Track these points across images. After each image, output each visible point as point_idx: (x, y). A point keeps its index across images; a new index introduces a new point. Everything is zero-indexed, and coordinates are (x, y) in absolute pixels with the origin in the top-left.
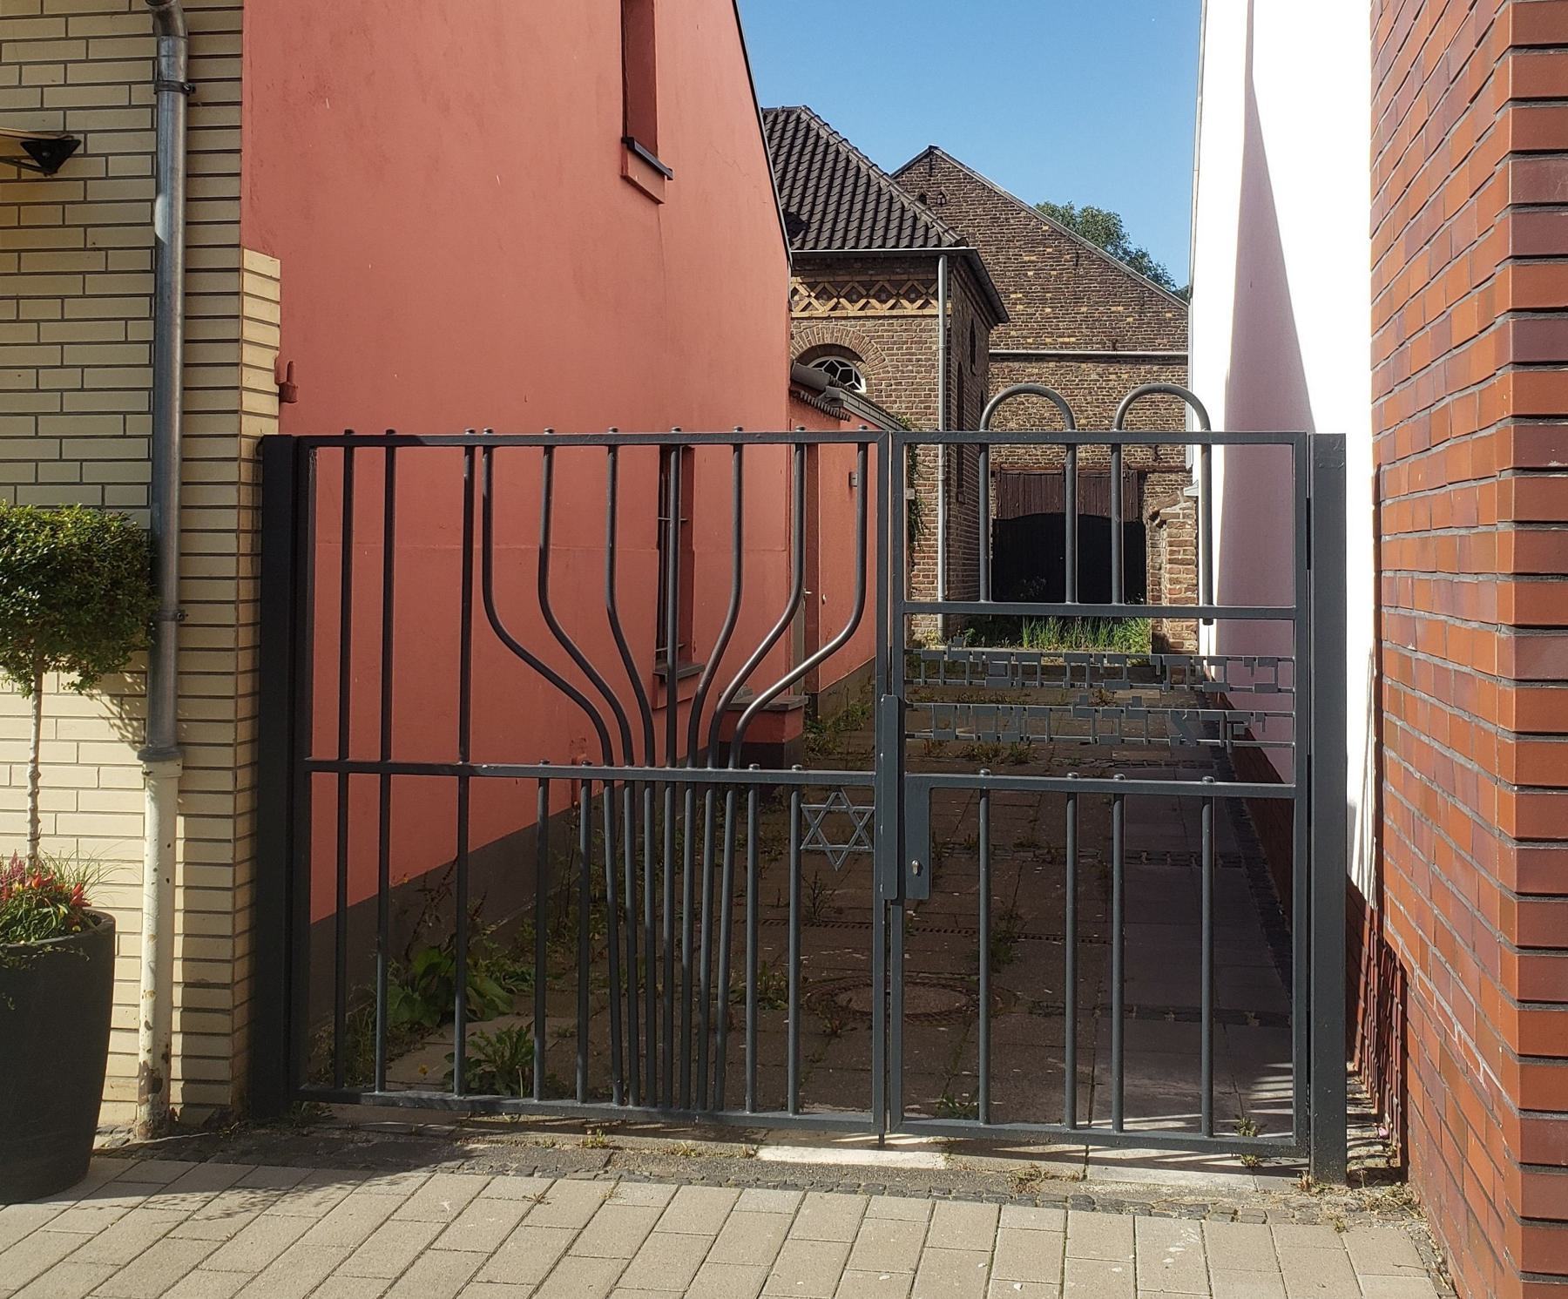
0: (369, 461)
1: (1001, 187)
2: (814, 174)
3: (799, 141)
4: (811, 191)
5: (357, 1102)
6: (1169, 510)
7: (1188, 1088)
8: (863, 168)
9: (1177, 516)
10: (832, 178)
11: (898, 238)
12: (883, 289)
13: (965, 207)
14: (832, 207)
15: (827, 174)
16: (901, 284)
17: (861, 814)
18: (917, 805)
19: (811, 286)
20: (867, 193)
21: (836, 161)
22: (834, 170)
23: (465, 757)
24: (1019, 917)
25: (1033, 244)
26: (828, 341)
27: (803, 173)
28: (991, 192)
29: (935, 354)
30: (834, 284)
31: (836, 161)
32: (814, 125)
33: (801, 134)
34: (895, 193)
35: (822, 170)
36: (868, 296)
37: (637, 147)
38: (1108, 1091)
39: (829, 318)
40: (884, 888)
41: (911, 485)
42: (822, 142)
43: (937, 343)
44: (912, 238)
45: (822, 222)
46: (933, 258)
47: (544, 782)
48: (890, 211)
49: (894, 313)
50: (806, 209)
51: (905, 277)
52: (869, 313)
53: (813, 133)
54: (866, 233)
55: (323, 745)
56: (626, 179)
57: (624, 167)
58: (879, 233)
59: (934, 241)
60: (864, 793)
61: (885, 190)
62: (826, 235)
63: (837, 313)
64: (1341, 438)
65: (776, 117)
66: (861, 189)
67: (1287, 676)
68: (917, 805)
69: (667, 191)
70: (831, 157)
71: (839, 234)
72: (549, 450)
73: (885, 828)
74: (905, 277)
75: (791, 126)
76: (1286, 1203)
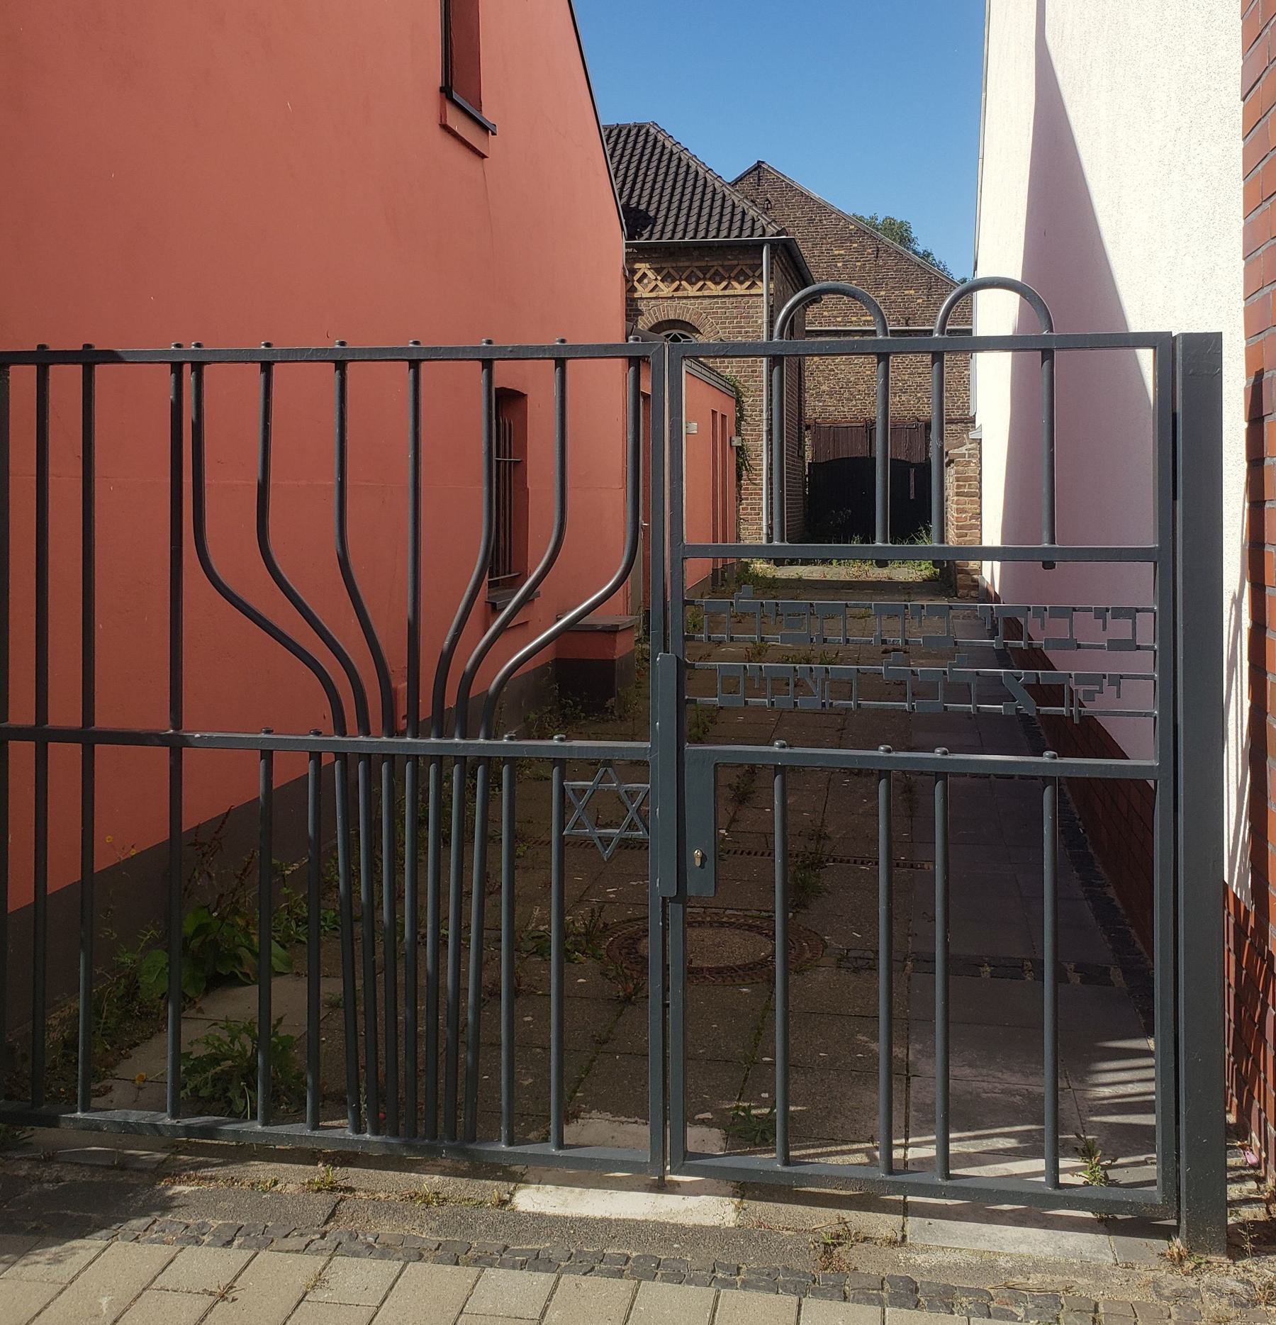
0: (66, 378)
1: (816, 194)
2: (660, 178)
3: (648, 151)
4: (657, 192)
5: (56, 1126)
6: (956, 451)
7: (1015, 1080)
8: (701, 172)
9: (963, 455)
10: (675, 181)
11: (730, 230)
12: (717, 273)
13: (786, 211)
14: (675, 205)
15: (671, 177)
16: (732, 268)
17: (632, 795)
18: (700, 785)
19: (658, 271)
20: (704, 193)
21: (678, 167)
22: (677, 174)
23: (177, 721)
24: (827, 837)
25: (843, 240)
26: (672, 317)
27: (652, 177)
28: (808, 198)
29: (760, 326)
30: (677, 269)
31: (678, 167)
32: (660, 137)
33: (650, 144)
34: (727, 192)
35: (666, 174)
36: (704, 279)
37: (455, 96)
38: (927, 1088)
39: (672, 297)
40: (661, 883)
41: (739, 433)
42: (667, 151)
43: (761, 317)
44: (741, 229)
45: (667, 217)
46: (758, 246)
47: (267, 755)
48: (723, 207)
49: (727, 292)
50: (653, 206)
51: (735, 262)
52: (706, 293)
53: (659, 144)
54: (703, 226)
55: (21, 712)
56: (445, 127)
57: (443, 115)
58: (714, 225)
59: (759, 232)
60: (638, 766)
61: (718, 190)
62: (669, 228)
63: (680, 294)
64: (1218, 337)
65: (630, 131)
66: (699, 190)
67: (1146, 630)
68: (700, 785)
69: (491, 145)
70: (674, 163)
71: (681, 227)
72: (267, 367)
73: (663, 812)
74: (735, 262)
75: (641, 138)
76: (1156, 1285)
